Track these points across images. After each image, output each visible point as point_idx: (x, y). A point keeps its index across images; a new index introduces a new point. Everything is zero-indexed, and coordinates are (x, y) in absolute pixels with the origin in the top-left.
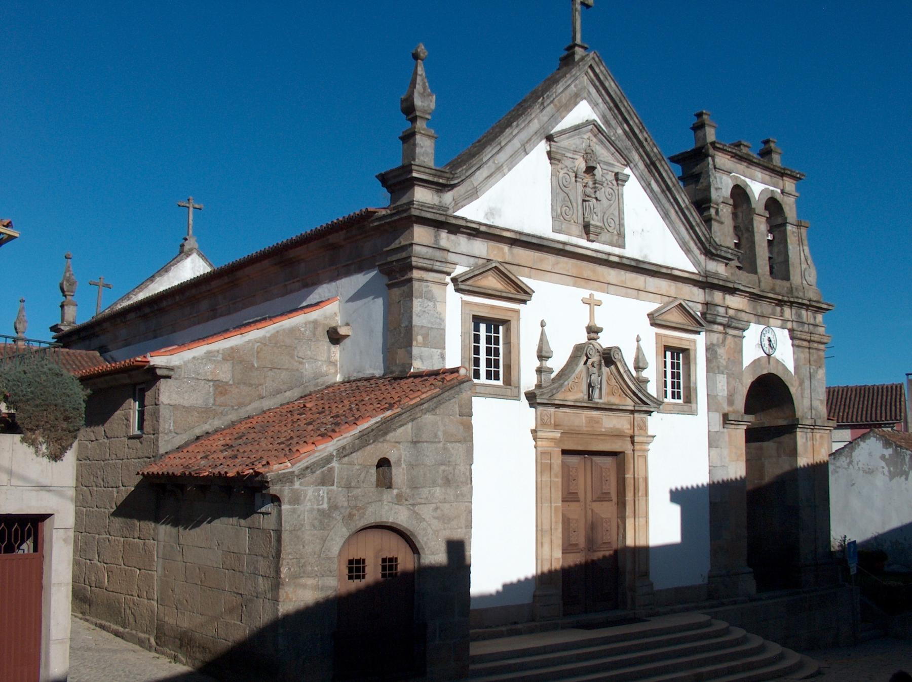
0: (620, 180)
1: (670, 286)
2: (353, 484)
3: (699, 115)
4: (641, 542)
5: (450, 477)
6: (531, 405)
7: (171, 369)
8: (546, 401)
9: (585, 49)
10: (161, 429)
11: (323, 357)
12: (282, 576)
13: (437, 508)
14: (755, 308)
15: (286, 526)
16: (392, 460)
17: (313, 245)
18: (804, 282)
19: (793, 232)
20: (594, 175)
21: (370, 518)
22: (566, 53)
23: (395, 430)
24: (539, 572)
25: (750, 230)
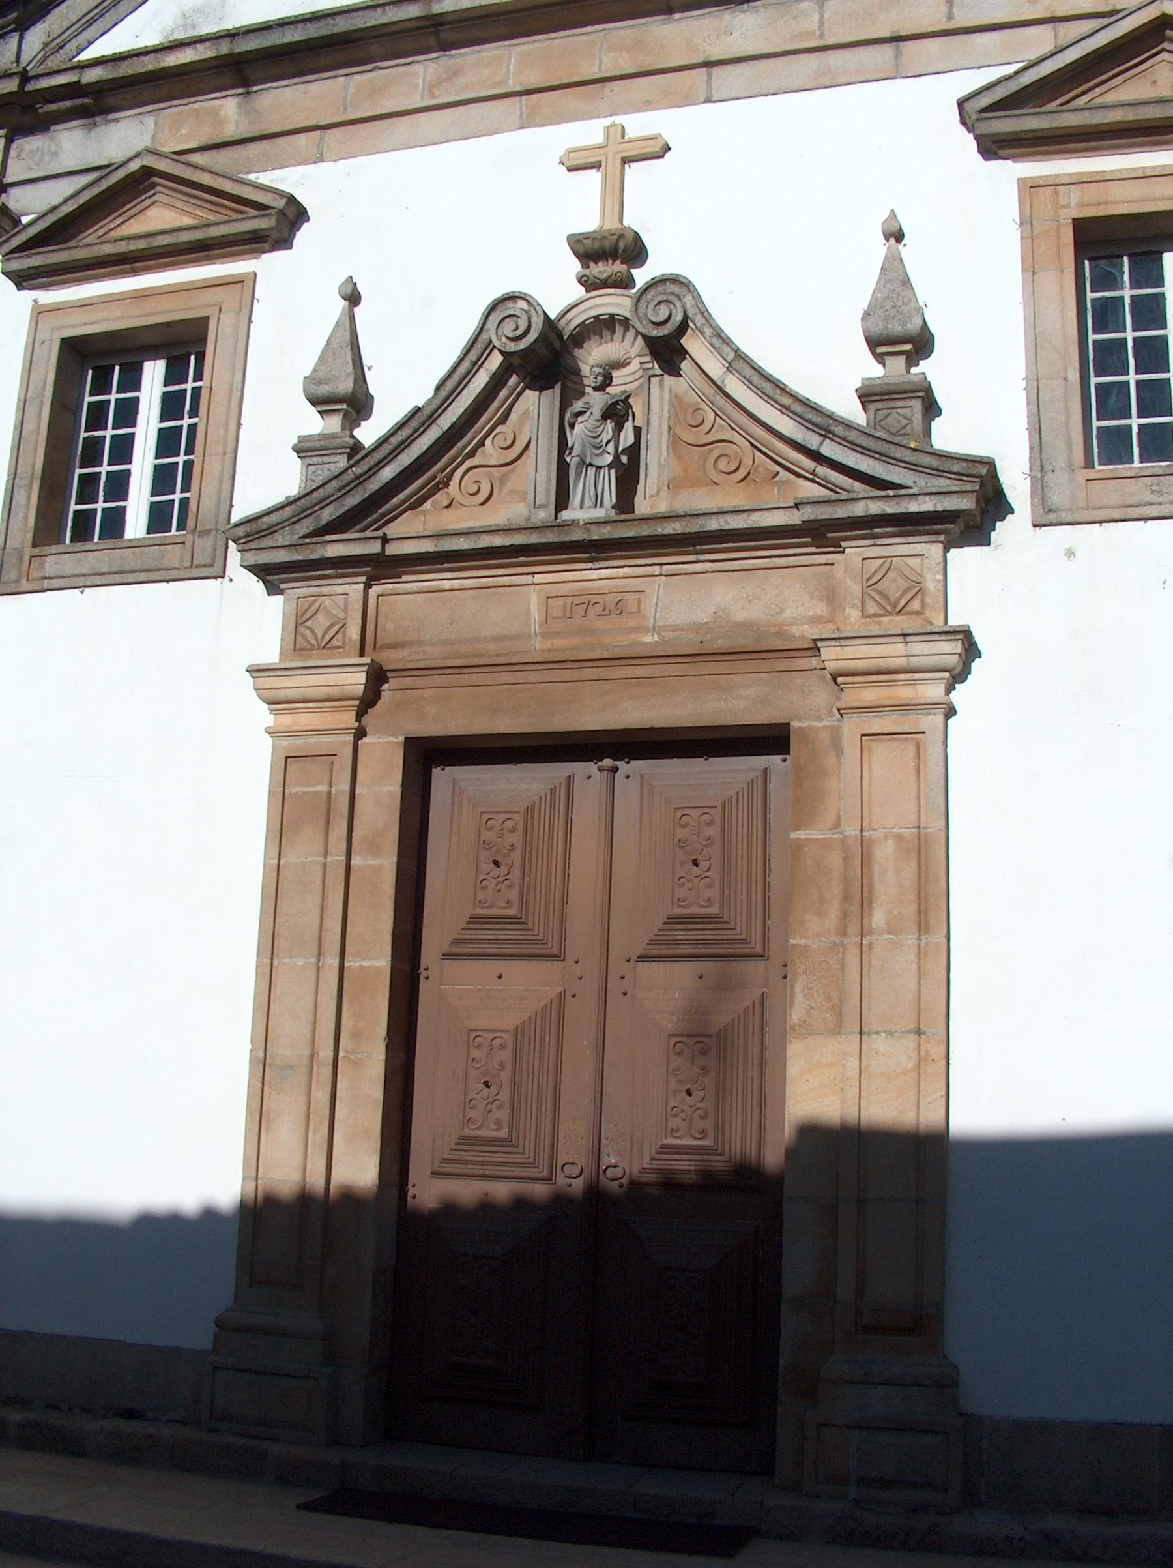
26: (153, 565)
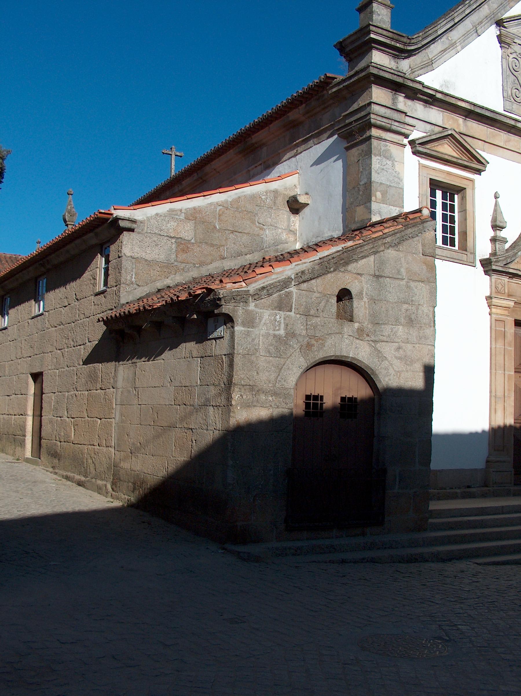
2: (312, 312)
5: (413, 317)
6: (486, 273)
7: (134, 221)
8: (500, 269)
10: (123, 280)
11: (283, 225)
12: (233, 403)
13: (399, 348)
15: (239, 349)
16: (354, 292)
17: (274, 126)
23: (356, 261)
26: (460, 259)
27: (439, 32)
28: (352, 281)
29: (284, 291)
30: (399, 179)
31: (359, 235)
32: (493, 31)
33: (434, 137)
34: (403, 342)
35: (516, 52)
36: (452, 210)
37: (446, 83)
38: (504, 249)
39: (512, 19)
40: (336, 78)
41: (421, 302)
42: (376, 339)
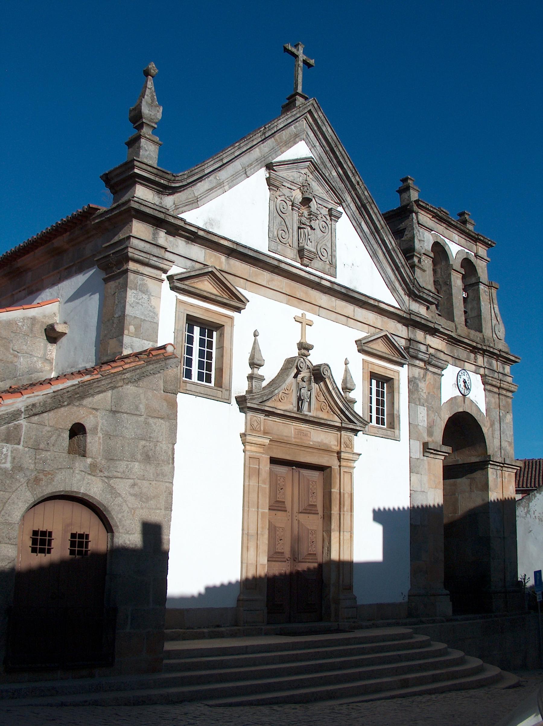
0: (333, 216)
1: (377, 319)
2: (42, 446)
3: (405, 180)
4: (345, 557)
6: (242, 410)
9: (306, 99)
11: (40, 354)
13: (134, 485)
14: (452, 351)
16: (88, 427)
17: (39, 251)
18: (494, 336)
19: (485, 291)
20: (310, 207)
21: (59, 485)
22: (287, 101)
23: (93, 395)
24: (244, 577)
25: (448, 284)
26: (215, 395)
27: (207, 172)
28: (87, 415)
29: (13, 424)
30: (155, 313)
31: (98, 370)
32: (263, 173)
33: (193, 274)
34: (139, 479)
35: (284, 195)
36: (210, 346)
37: (211, 222)
38: (261, 387)
39: (282, 163)
40: (99, 209)
41: (160, 439)
42: (110, 474)
